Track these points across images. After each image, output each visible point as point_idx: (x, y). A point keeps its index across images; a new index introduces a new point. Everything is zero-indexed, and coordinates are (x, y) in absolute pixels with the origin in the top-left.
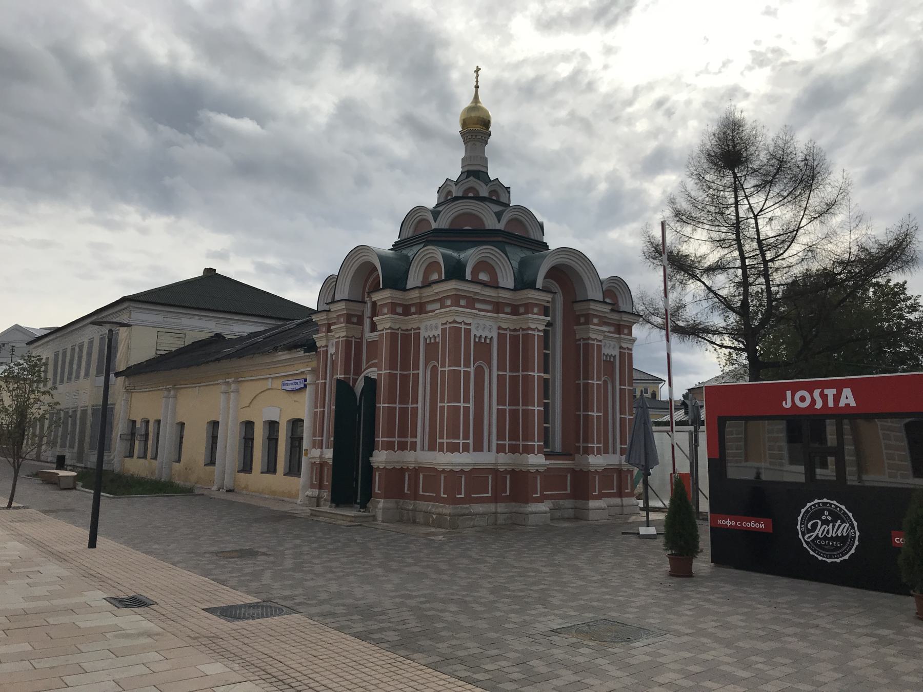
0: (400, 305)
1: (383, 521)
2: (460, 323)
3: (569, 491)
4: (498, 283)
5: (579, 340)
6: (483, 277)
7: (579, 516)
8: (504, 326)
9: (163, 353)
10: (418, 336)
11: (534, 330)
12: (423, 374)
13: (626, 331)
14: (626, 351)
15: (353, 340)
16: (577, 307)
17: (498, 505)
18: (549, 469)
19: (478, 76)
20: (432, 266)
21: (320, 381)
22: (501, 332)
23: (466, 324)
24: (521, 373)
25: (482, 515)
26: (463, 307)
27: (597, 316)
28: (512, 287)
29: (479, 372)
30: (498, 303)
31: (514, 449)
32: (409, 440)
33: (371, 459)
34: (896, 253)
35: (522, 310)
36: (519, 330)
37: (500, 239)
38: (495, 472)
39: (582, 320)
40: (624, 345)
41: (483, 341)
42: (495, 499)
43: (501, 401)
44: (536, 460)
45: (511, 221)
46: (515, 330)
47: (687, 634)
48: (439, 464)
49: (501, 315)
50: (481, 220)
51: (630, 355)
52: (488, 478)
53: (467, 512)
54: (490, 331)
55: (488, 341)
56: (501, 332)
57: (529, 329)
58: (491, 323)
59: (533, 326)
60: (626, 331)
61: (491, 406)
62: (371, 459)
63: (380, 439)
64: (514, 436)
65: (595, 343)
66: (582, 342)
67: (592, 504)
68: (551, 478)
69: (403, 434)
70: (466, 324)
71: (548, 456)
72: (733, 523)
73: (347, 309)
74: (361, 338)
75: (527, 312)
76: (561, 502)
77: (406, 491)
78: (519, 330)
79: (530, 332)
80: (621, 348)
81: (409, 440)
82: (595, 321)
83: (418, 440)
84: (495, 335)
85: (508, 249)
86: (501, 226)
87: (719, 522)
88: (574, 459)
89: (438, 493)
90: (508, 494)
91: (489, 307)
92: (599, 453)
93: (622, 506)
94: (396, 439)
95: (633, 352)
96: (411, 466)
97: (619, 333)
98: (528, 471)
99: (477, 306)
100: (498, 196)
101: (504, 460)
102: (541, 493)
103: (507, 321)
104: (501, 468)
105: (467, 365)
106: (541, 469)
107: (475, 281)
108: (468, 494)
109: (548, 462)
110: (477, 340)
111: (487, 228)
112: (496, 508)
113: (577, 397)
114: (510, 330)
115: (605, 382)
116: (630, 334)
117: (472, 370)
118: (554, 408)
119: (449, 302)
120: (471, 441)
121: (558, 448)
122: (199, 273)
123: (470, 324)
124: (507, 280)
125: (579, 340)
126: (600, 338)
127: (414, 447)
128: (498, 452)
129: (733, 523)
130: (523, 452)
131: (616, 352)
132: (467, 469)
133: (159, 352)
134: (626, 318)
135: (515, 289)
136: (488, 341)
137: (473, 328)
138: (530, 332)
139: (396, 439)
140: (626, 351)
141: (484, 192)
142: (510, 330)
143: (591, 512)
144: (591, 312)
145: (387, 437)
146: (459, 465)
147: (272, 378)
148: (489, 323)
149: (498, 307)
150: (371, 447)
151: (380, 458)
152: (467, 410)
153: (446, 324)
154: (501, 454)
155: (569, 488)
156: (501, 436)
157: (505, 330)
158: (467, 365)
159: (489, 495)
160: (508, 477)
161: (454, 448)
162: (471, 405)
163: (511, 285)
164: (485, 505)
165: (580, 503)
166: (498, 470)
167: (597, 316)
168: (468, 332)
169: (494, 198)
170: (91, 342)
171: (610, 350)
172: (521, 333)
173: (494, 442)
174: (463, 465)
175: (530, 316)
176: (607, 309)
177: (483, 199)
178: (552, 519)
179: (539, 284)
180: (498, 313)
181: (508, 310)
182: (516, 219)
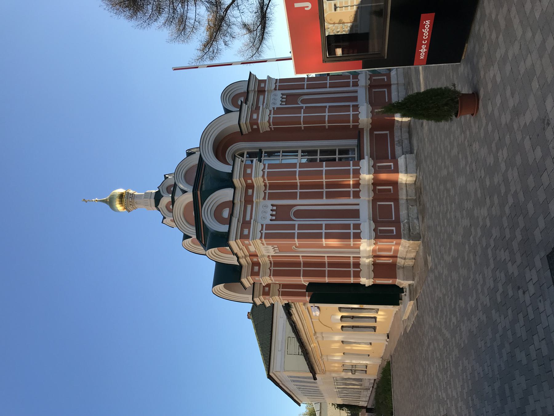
2: (262, 234)
3: (388, 132)
4: (244, 93)
5: (271, 128)
6: (226, 213)
8: (262, 195)
9: (300, 350)
13: (262, 85)
15: (281, 290)
16: (245, 131)
18: (371, 156)
22: (277, 88)
26: (249, 232)
28: (232, 190)
29: (300, 214)
32: (352, 269)
33: (367, 285)
36: (265, 183)
39: (255, 127)
41: (274, 213)
43: (319, 196)
45: (187, 181)
47: (509, 11)
48: (366, 83)
50: (189, 203)
51: (282, 80)
53: (407, 225)
54: (266, 206)
55: (275, 208)
56: (277, 88)
57: (269, 122)
59: (267, 119)
60: (262, 85)
61: (323, 203)
62: (367, 285)
63: (352, 280)
65: (272, 116)
66: (272, 127)
69: (347, 265)
70: (262, 229)
72: (424, 47)
73: (259, 296)
75: (257, 124)
79: (271, 121)
80: (275, 89)
82: (255, 116)
86: (190, 189)
87: (422, 58)
91: (249, 207)
99: (248, 218)
100: (170, 186)
103: (258, 197)
105: (292, 227)
106: (372, 163)
107: (229, 222)
109: (366, 157)
110: (274, 218)
111: (192, 200)
112: (394, 84)
115: (303, 101)
116: (264, 81)
120: (351, 104)
121: (354, 142)
122: (250, 322)
123: (262, 225)
125: (271, 128)
126: (268, 111)
129: (424, 47)
131: (279, 93)
132: (370, 108)
133: (300, 353)
134: (252, 87)
136: (275, 208)
138: (271, 121)
139: (352, 269)
142: (265, 190)
145: (350, 174)
146: (370, 232)
149: (248, 200)
152: (331, 108)
158: (292, 227)
159: (386, 90)
162: (324, 222)
163: (231, 191)
164: (401, 207)
168: (268, 227)
169: (172, 189)
170: (296, 385)
171: (276, 99)
172: (267, 182)
173: (351, 200)
174: (369, 165)
175: (259, 121)
176: (245, 107)
178: (411, 152)
179: (227, 169)
181: (250, 191)
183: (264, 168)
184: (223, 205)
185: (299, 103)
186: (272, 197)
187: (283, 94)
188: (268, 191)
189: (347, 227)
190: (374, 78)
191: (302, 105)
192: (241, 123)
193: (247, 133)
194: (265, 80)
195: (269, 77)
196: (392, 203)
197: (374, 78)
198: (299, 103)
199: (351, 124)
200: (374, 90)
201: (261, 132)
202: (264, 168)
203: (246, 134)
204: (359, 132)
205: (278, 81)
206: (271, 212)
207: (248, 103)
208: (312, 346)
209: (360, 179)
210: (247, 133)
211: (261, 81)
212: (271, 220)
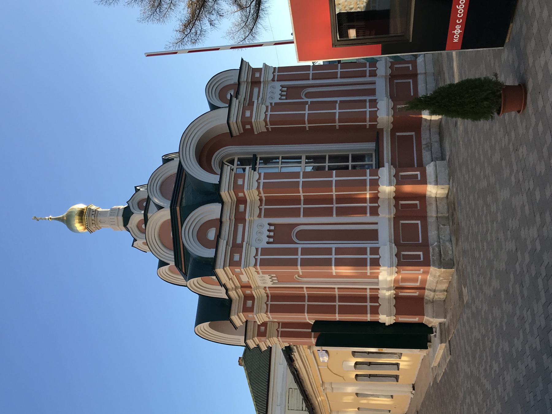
0: (245, 303)
1: (445, 318)
3: (413, 133)
4: (234, 84)
5: (267, 129)
6: (212, 234)
8: (257, 212)
9: (304, 405)
13: (257, 75)
15: (280, 330)
16: (235, 132)
17: (418, 72)
18: (393, 163)
22: (276, 79)
25: (438, 229)
27: (243, 113)
33: (387, 324)
36: (261, 197)
39: (248, 127)
40: (271, 77)
41: (272, 234)
43: (328, 212)
48: (386, 72)
49: (262, 80)
51: (281, 69)
52: (401, 175)
53: (437, 249)
54: (262, 226)
55: (272, 228)
56: (276, 79)
57: (265, 120)
58: (269, 87)
59: (263, 116)
60: (257, 75)
61: (333, 222)
62: (387, 324)
63: (369, 318)
65: (269, 113)
66: (269, 126)
69: (363, 298)
70: (257, 255)
71: (380, 164)
75: (250, 123)
76: (424, 142)
79: (268, 120)
80: (273, 80)
82: (248, 114)
86: (166, 204)
91: (240, 226)
93: (425, 73)
94: (369, 304)
95: (277, 66)
99: (239, 241)
100: (143, 200)
104: (389, 71)
106: (393, 171)
107: (216, 245)
108: (417, 247)
109: (386, 165)
110: (271, 240)
111: (169, 217)
114: (261, 205)
115: (308, 95)
116: (259, 70)
117: (300, 246)
118: (333, 151)
120: (368, 98)
121: (370, 146)
124: (211, 211)
125: (267, 129)
126: (264, 108)
130: (377, 121)
131: (278, 85)
132: (395, 250)
133: (304, 409)
134: (244, 78)
136: (272, 228)
137: (273, 102)
138: (268, 120)
139: (369, 304)
142: (261, 205)
145: (366, 186)
146: (391, 258)
147: (318, 366)
148: (255, 229)
149: (240, 218)
150: (377, 324)
154: (380, 211)
158: (294, 251)
162: (333, 245)
164: (429, 227)
167: (243, 113)
168: (265, 251)
169: (145, 204)
171: (274, 92)
172: (263, 195)
173: (368, 79)
174: (390, 175)
175: (253, 120)
177: (146, 220)
178: (443, 158)
181: (242, 207)
185: (303, 97)
186: (269, 214)
191: (306, 100)
192: (231, 122)
193: (238, 134)
195: (265, 65)
196: (419, 222)
197: (396, 66)
201: (256, 133)
202: (259, 178)
204: (378, 133)
210: (238, 134)
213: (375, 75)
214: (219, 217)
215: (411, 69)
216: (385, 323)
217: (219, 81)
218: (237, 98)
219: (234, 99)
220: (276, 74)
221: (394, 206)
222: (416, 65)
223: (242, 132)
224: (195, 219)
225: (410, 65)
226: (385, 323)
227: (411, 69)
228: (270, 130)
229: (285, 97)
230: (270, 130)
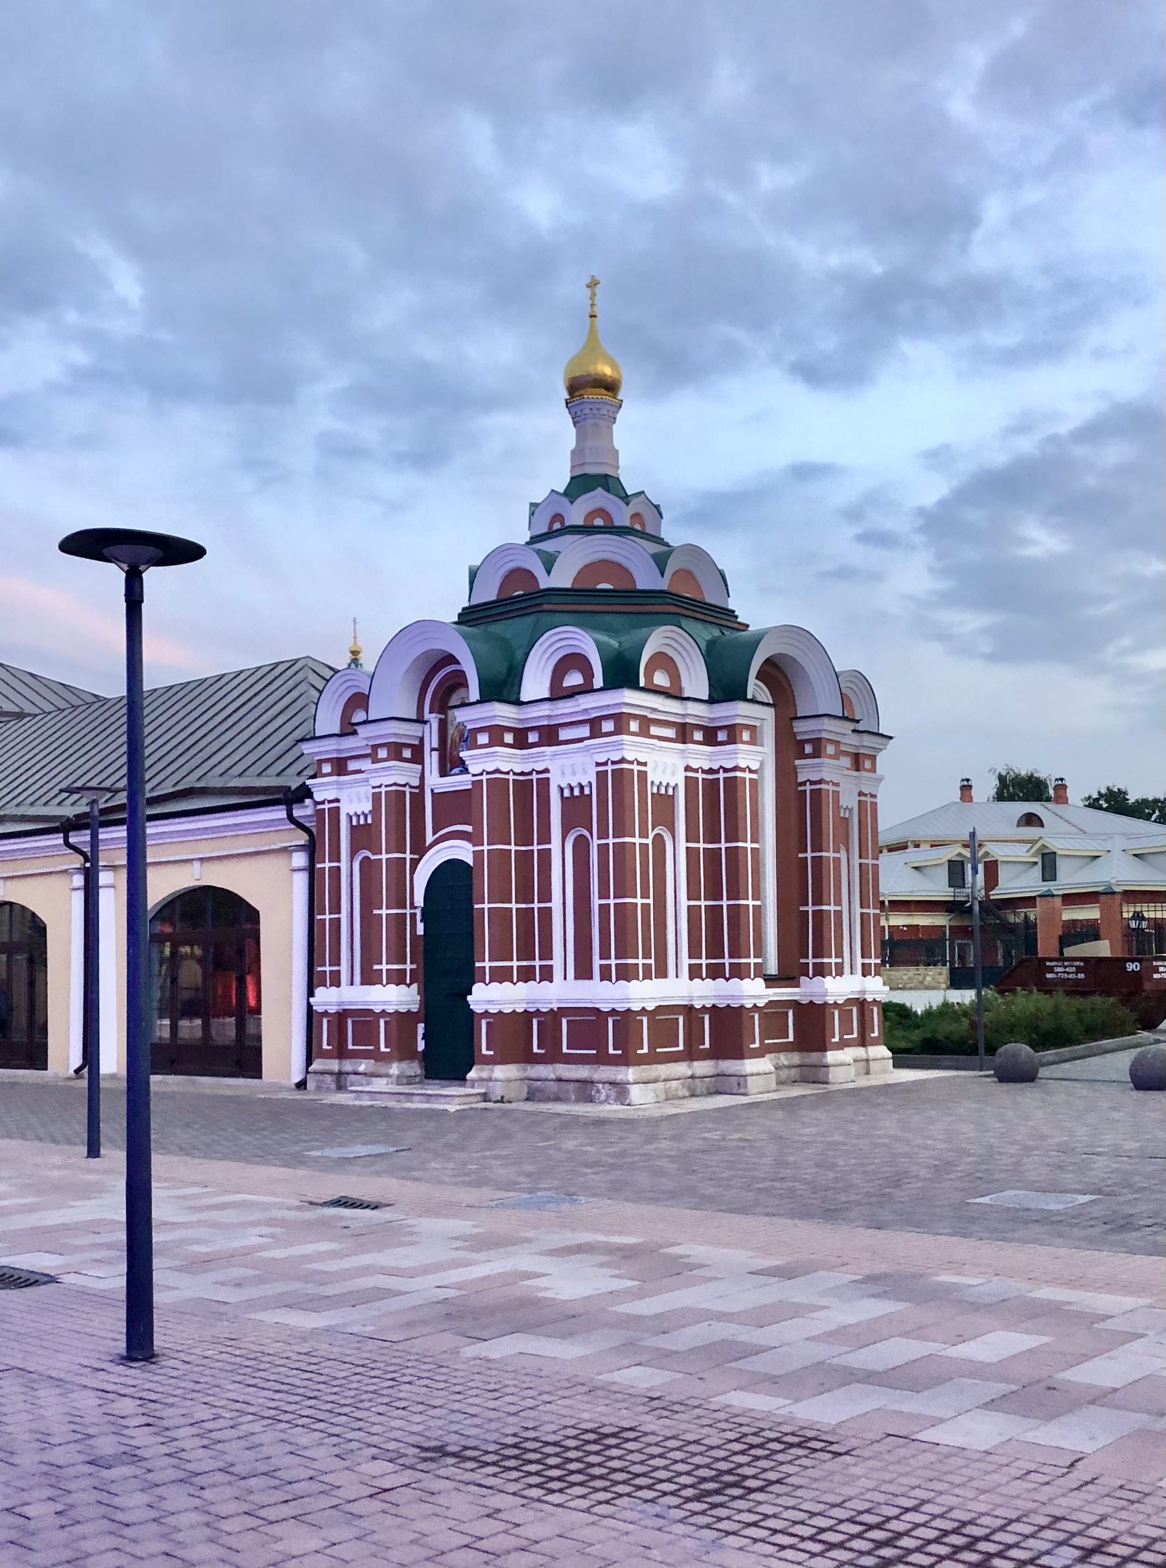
3: (791, 1039)
4: (681, 689)
7: (814, 1075)
10: (544, 784)
11: (743, 770)
12: (560, 852)
13: (868, 764)
14: (868, 799)
16: (800, 727)
18: (771, 1004)
19: (594, 295)
20: (573, 661)
21: (327, 865)
22: (862, 798)
23: (639, 763)
24: (723, 845)
30: (684, 725)
31: (715, 972)
32: (537, 963)
33: (469, 998)
34: (572, 503)
35: (722, 736)
36: (717, 772)
37: (672, 609)
38: (688, 1010)
39: (808, 749)
42: (690, 1055)
44: (752, 992)
46: (711, 771)
48: (871, 993)
51: (874, 805)
64: (715, 950)
67: (831, 1056)
68: (773, 1014)
70: (639, 763)
74: (421, 786)
75: (816, 754)
77: (535, 1050)
78: (717, 772)
79: (625, 766)
80: (861, 794)
81: (537, 963)
83: (344, 968)
84: (679, 779)
85: (684, 622)
86: (663, 584)
88: (798, 986)
89: (601, 1045)
90: (707, 1045)
92: (648, 976)
94: (727, 961)
95: (877, 800)
96: (332, 1010)
97: (858, 770)
98: (742, 1007)
99: (654, 730)
100: (643, 524)
101: (706, 992)
102: (761, 1041)
103: (701, 756)
104: (869, 998)
106: (761, 1003)
113: (802, 882)
115: (659, 839)
119: (608, 726)
124: (696, 682)
125: (804, 783)
127: (547, 974)
128: (691, 979)
134: (868, 740)
135: (711, 701)
136: (670, 792)
138: (739, 774)
140: (868, 799)
141: (622, 518)
142: (704, 772)
143: (831, 1069)
144: (824, 735)
149: (684, 733)
150: (469, 977)
151: (485, 997)
153: (605, 764)
155: (876, 1028)
156: (694, 952)
157: (696, 771)
159: (681, 1048)
160: (707, 1018)
161: (626, 973)
165: (814, 1057)
166: (692, 1006)
169: (637, 527)
173: (686, 961)
180: (684, 743)
182: (688, 572)
183: (751, 771)
184: (675, 676)
185: (656, 831)
186: (690, 783)
187: (851, 810)
188: (700, 776)
189: (547, 953)
190: (756, 1016)
191: (651, 836)
192: (826, 720)
193: (795, 730)
194: (875, 772)
195: (880, 780)
196: (681, 1048)
197: (756, 1016)
198: (656, 831)
199: (811, 961)
200: (855, 1010)
201: (797, 762)
202: (751, 771)
203: (792, 727)
204: (793, 978)
205: (873, 800)
206: (664, 784)
207: (855, 736)
208: (226, 862)
209: (727, 980)
210: (795, 730)
211: (873, 758)
212: (652, 783)
213: (864, 975)
214: (799, 715)
215: (752, 1046)
216: (471, 994)
217: (683, 647)
218: (854, 731)
219: (852, 726)
220: (636, 768)
221: (704, 1006)
222: (616, 1065)
223: (798, 738)
224: (683, 647)
225: (645, 1050)
226: (471, 994)
227: (752, 1046)
228: (800, 788)
229: (655, 791)
230: (800, 788)
